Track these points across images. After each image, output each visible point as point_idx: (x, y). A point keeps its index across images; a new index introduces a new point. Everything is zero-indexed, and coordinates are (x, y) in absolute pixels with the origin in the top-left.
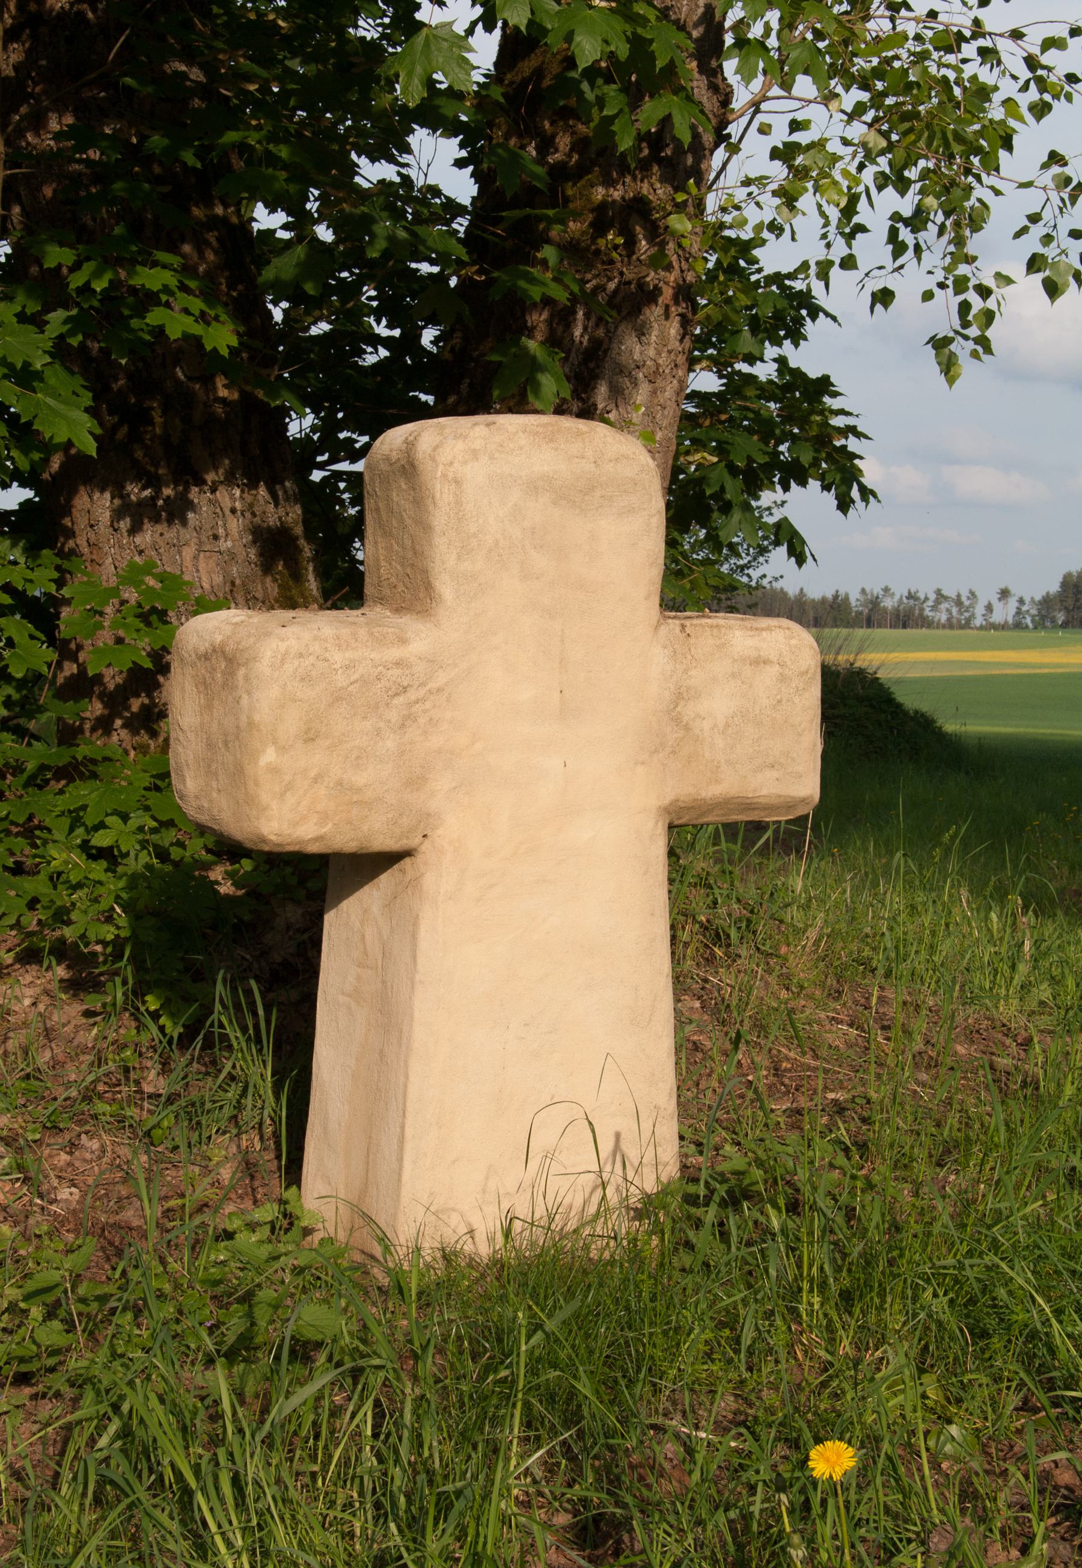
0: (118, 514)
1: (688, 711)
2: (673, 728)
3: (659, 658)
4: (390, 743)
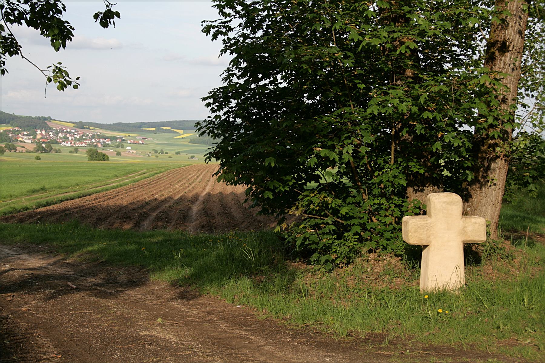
0: (413, 191)
1: (465, 229)
2: (463, 231)
3: (461, 223)
4: (425, 232)
